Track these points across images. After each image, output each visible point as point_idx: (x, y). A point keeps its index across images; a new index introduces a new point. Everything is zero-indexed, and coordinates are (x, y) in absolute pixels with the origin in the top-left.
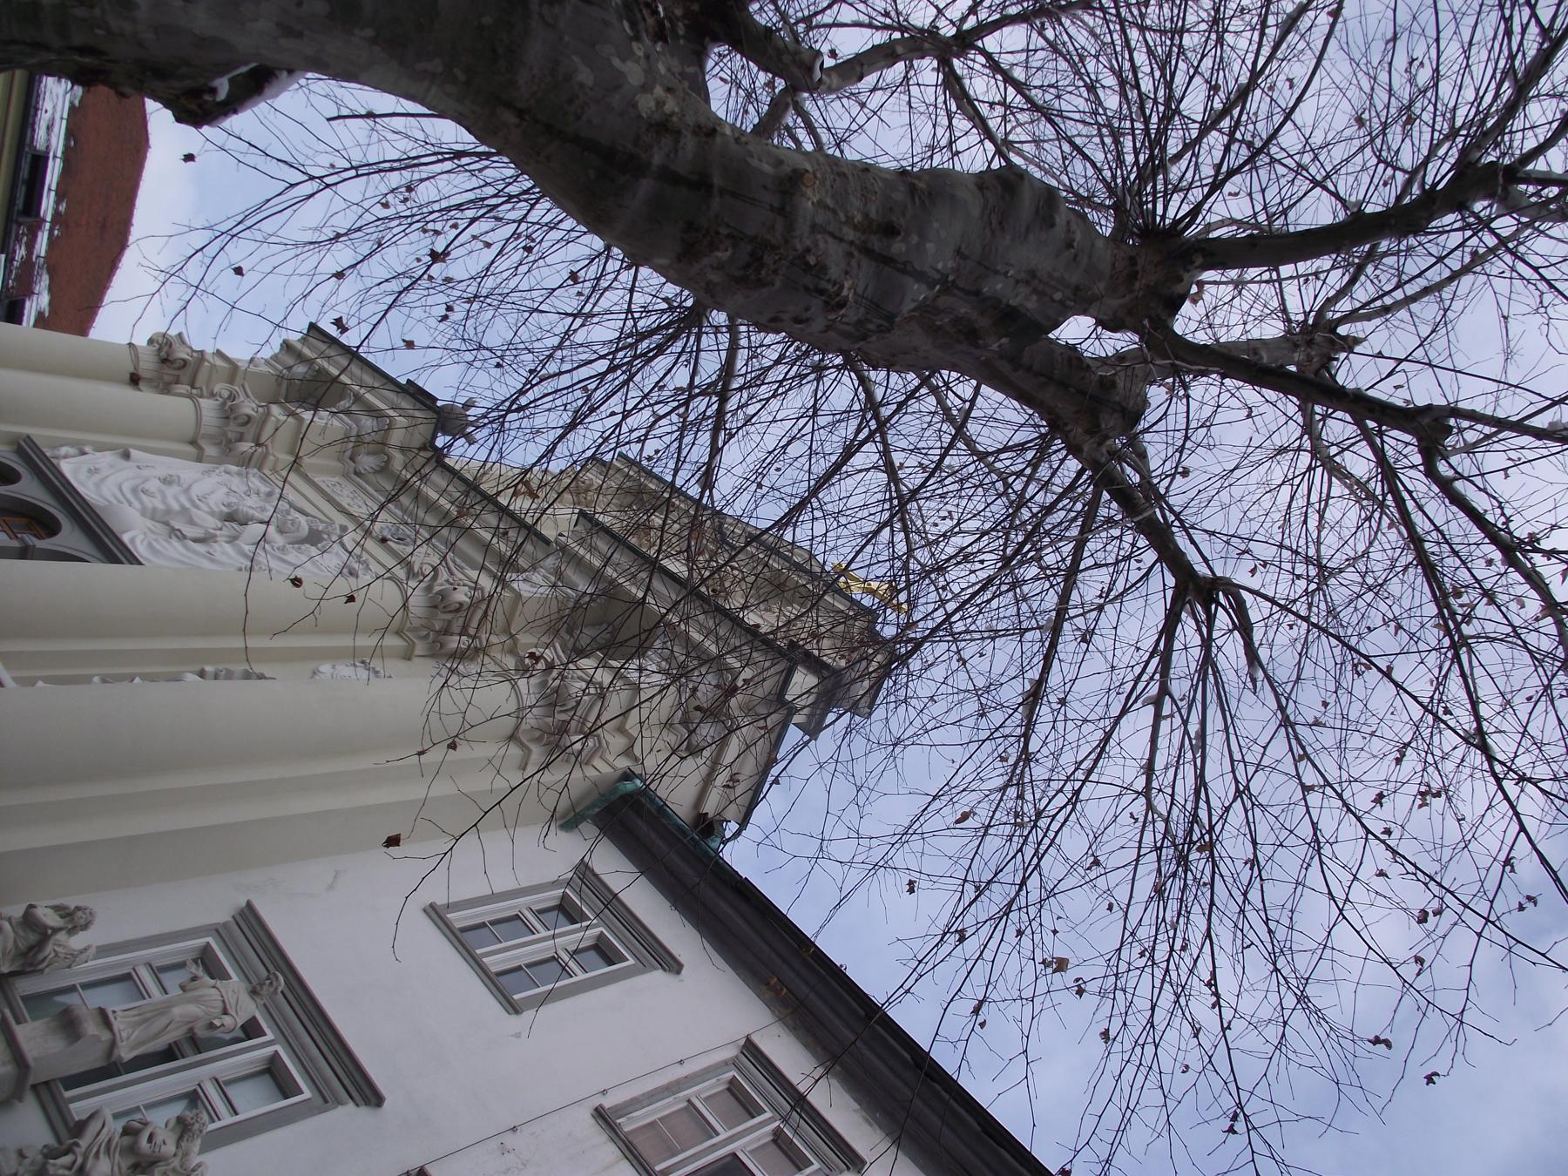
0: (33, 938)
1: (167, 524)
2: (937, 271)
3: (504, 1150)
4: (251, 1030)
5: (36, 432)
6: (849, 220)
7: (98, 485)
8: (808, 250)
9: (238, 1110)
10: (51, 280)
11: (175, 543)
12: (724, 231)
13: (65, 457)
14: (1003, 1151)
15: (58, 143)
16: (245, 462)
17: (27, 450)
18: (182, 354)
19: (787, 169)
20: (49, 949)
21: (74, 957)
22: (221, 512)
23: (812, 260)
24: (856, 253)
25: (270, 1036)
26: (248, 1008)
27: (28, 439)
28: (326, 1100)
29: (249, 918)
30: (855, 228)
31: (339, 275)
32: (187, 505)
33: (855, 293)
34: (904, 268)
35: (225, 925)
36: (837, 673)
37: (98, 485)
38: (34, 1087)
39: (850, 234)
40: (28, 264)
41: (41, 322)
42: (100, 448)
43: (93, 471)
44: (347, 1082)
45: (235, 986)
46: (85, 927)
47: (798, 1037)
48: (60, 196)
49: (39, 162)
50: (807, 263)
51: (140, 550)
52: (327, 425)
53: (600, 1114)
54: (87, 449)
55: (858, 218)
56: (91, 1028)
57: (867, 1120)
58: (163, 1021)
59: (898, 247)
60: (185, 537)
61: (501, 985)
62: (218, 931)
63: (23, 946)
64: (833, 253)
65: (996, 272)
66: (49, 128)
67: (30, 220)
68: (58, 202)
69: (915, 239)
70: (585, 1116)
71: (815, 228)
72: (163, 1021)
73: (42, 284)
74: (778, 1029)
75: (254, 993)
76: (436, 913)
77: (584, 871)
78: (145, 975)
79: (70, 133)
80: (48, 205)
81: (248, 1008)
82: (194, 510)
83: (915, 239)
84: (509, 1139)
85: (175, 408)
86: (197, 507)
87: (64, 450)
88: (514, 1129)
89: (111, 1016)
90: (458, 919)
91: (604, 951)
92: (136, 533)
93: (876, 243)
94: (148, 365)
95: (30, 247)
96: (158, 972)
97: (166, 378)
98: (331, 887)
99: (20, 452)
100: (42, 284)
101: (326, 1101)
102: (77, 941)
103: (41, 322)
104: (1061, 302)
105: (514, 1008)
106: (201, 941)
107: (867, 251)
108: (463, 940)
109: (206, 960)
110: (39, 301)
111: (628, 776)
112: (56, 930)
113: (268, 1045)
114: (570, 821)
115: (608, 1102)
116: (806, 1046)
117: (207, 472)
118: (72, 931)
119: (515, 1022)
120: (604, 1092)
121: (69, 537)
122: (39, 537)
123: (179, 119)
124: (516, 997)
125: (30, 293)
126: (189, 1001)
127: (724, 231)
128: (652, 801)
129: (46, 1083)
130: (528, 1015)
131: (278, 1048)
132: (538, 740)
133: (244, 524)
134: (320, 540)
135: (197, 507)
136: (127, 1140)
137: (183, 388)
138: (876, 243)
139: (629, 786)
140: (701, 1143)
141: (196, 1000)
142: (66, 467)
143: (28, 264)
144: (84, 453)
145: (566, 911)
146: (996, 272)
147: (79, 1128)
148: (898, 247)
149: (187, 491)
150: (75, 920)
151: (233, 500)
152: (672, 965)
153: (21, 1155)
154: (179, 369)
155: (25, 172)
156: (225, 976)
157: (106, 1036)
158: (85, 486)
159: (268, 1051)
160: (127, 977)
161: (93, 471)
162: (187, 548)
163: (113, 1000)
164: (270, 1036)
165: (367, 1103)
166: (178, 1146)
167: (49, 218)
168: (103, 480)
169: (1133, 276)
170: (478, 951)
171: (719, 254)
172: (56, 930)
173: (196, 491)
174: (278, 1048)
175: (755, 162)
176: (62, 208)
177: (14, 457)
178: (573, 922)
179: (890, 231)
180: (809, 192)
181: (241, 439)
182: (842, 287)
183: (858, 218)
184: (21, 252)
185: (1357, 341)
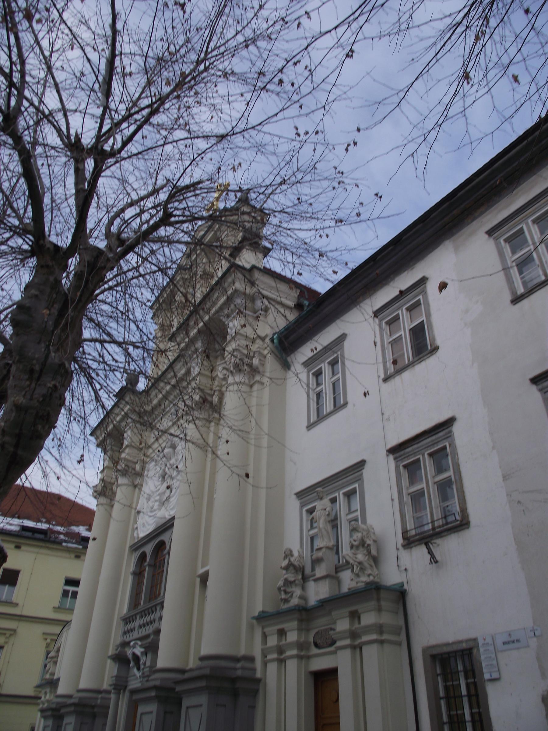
0: (291, 568)
1: (164, 502)
2: (45, 350)
3: (388, 419)
4: (333, 501)
5: (128, 544)
6: (29, 386)
7: (149, 525)
8: (38, 401)
9: (356, 509)
10: (73, 525)
11: (171, 500)
12: (32, 428)
13: (138, 534)
14: (432, 216)
15: (16, 521)
16: (143, 468)
17: (135, 548)
18: (100, 488)
19: (14, 408)
20: (296, 563)
21: (301, 556)
22: (162, 481)
23: (41, 399)
24: (39, 383)
25: (337, 494)
26: (326, 502)
27: (131, 547)
28: (360, 479)
29: (300, 495)
30: (31, 384)
31: (58, 478)
32: (158, 493)
33: (52, 380)
34: (44, 364)
35: (301, 503)
36: (244, 239)
37: (149, 525)
38: (336, 572)
39: (33, 385)
40: (66, 534)
41: (89, 530)
42: (135, 522)
43: (144, 525)
44: (356, 471)
45: (318, 505)
46: (291, 551)
47: (378, 290)
48: (38, 521)
49: (24, 528)
50: (42, 401)
51: (172, 513)
52: (129, 436)
53: (385, 380)
54: (135, 526)
55: (28, 383)
56: (320, 554)
57: (412, 269)
58: (323, 530)
59: (37, 368)
60: (169, 496)
61: (338, 407)
62: (302, 506)
63: (293, 571)
64: (41, 391)
65: (46, 327)
66: (11, 525)
67: (49, 533)
68: (42, 522)
69: (34, 362)
70: (386, 387)
71: (31, 399)
72: (323, 530)
73: (75, 529)
74: (373, 298)
75: (321, 499)
76: (310, 426)
77: (306, 364)
78: (312, 532)
79: (13, 517)
80: (44, 526)
81: (326, 502)
82: (160, 491)
83: (34, 362)
84: (386, 416)
85: (121, 493)
86: (159, 490)
87: (135, 535)
88: (383, 414)
89: (318, 547)
90: (313, 418)
91: (334, 363)
92: (165, 514)
93: (36, 375)
94: (103, 500)
95: (59, 533)
96: (312, 527)
97: (110, 493)
98: (295, 464)
99: (136, 550)
100: (75, 529)
101: (360, 479)
102: (296, 554)
103: (89, 530)
104: (57, 294)
105: (346, 404)
106: (304, 512)
107: (38, 379)
108: (321, 417)
109: (311, 511)
110: (82, 530)
111: (272, 340)
112: (290, 561)
113: (340, 495)
114: (286, 366)
115: (382, 376)
116: (382, 287)
117: (147, 484)
118: (292, 555)
119: (350, 406)
120: (379, 377)
121: (164, 537)
122: (165, 548)
123: (6, 561)
124: (342, 402)
125: (78, 534)
126: (319, 521)
127: (32, 428)
128: (283, 332)
129: (336, 569)
130: (349, 399)
131: (341, 492)
132: (254, 377)
133: (166, 474)
134: (174, 444)
135: (159, 490)
136: (354, 548)
137: (114, 487)
138: (36, 375)
139: (276, 341)
140: (403, 342)
141: (320, 518)
142: (142, 535)
143: (66, 534)
144: (137, 528)
145: (318, 374)
146: (46, 327)
147: (347, 562)
148: (37, 368)
149: (153, 492)
150: (289, 554)
151: (157, 475)
152: (343, 337)
153: (352, 580)
154: (107, 488)
155: (29, 534)
156: (315, 507)
157: (324, 550)
158: (149, 529)
159: (341, 496)
160: (312, 539)
161: (144, 525)
162: (173, 496)
163: (318, 543)
164: (337, 494)
165: (364, 465)
166: (360, 532)
167: (48, 526)
168: (147, 523)
169: (47, 266)
170: (325, 413)
171: (39, 429)
172: (290, 561)
173: (153, 489)
174: (341, 492)
175: (12, 419)
176: (44, 520)
177: (137, 552)
178: (322, 373)
179: (32, 371)
180: (20, 402)
181: (134, 469)
182: (50, 387)
183: (28, 383)
184: (62, 537)
185: (77, 135)
